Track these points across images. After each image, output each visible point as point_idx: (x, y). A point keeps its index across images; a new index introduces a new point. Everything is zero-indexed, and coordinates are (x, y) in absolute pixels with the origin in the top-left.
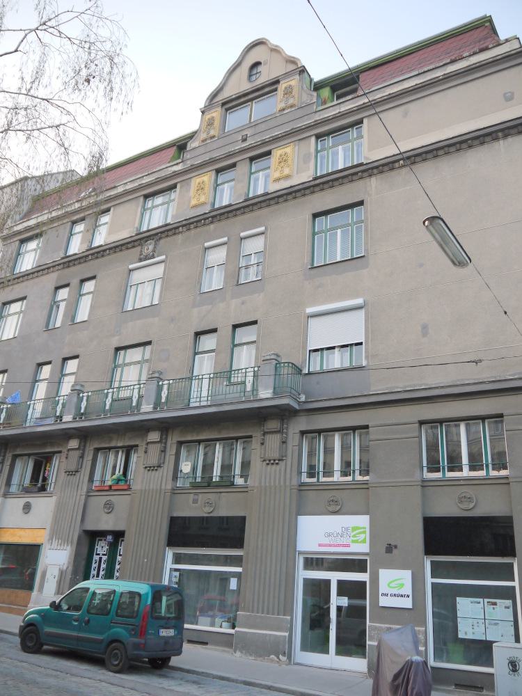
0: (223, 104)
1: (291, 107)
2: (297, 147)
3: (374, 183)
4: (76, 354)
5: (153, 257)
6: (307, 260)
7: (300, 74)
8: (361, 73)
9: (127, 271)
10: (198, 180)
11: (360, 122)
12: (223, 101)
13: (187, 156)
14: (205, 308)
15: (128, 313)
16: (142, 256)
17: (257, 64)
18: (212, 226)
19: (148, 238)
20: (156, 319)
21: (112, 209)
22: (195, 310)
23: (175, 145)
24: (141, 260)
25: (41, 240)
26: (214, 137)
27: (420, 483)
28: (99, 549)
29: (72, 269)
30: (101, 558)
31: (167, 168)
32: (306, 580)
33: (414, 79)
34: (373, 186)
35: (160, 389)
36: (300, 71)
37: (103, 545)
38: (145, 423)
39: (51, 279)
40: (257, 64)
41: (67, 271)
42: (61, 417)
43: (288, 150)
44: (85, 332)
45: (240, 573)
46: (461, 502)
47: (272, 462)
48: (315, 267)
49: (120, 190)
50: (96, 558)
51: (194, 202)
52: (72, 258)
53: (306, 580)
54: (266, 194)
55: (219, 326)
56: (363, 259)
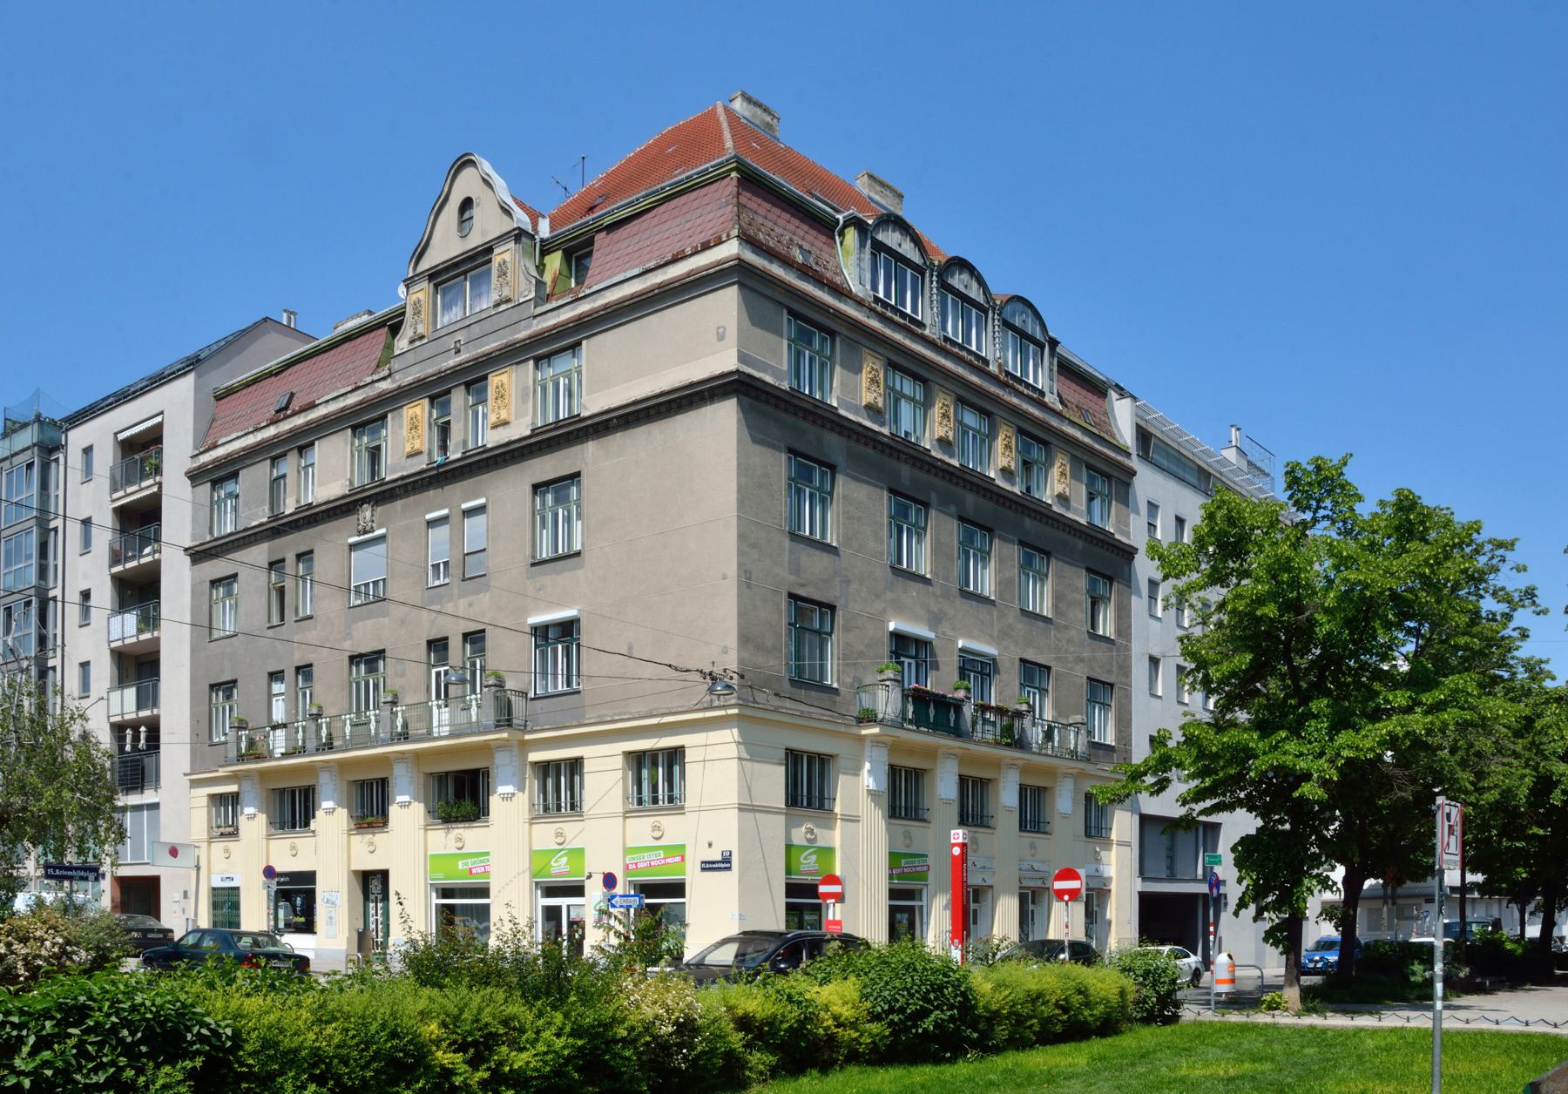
1: (508, 301)
2: (514, 375)
3: (591, 448)
4: (308, 663)
6: (528, 551)
8: (597, 232)
10: (411, 412)
11: (579, 344)
13: (396, 364)
16: (360, 527)
23: (384, 325)
26: (422, 337)
28: (374, 888)
32: (436, 905)
34: (590, 451)
35: (319, 727)
36: (515, 235)
43: (504, 378)
44: (314, 632)
46: (653, 831)
53: (436, 905)
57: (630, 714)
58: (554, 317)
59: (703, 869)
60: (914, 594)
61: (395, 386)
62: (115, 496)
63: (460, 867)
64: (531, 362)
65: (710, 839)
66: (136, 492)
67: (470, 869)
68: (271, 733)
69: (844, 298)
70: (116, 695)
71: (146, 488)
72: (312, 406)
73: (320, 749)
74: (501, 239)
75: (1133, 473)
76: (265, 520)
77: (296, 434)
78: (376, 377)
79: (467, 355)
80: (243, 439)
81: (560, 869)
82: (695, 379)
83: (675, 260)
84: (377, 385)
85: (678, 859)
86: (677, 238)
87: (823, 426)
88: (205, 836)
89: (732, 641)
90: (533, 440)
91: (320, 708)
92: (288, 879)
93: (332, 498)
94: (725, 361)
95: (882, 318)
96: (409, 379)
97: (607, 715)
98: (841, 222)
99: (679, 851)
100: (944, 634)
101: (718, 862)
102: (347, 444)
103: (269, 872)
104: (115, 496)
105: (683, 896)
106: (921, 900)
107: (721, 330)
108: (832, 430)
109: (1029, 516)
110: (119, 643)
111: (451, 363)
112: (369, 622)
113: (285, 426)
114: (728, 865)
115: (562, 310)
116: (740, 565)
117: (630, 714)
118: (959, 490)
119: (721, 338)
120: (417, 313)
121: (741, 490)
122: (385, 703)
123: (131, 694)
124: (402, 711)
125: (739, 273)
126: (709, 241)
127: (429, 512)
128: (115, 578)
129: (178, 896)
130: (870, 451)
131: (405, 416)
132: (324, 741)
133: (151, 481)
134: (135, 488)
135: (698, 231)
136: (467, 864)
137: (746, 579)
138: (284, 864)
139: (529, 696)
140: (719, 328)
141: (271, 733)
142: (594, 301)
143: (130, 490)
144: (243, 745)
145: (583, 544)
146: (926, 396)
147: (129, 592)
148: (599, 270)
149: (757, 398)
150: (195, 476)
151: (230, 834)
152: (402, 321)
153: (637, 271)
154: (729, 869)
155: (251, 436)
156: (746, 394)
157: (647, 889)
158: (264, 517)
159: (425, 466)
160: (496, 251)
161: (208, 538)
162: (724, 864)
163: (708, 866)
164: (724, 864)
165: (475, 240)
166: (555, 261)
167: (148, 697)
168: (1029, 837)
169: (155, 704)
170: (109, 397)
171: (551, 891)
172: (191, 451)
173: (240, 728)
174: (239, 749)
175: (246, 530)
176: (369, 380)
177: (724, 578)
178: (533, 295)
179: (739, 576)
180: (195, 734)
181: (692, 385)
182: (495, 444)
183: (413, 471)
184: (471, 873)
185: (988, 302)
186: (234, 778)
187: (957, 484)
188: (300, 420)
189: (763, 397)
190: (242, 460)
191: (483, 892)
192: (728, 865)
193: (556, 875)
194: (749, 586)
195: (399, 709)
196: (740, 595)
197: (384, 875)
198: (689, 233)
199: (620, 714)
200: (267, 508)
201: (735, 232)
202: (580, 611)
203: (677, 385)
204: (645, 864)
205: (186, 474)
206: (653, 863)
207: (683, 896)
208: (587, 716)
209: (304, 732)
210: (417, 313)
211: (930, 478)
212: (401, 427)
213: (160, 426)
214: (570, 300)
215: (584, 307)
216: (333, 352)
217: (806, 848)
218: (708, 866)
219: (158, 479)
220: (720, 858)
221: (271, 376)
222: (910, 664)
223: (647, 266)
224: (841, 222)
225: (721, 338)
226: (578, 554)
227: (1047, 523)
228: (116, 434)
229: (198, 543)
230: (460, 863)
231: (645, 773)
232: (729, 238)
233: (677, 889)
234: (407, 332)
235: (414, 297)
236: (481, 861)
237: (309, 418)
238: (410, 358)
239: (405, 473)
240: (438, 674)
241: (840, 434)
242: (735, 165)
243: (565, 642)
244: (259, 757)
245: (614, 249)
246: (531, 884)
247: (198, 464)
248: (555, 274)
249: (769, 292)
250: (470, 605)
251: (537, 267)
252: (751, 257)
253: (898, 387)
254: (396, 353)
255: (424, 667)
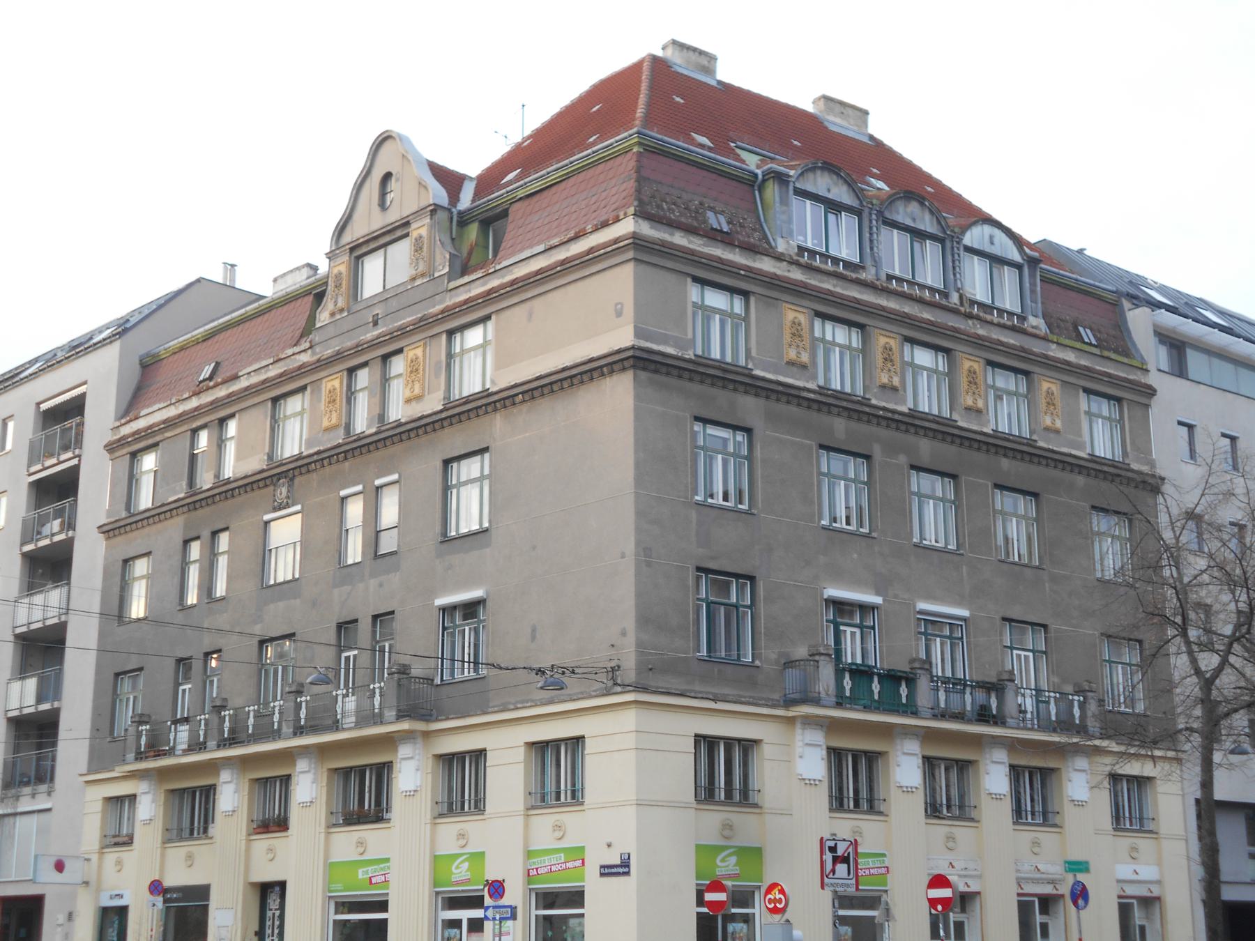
0: (352, 250)
5: (287, 506)
6: (438, 529)
7: (431, 215)
9: (262, 524)
10: (329, 385)
12: (351, 245)
13: (316, 337)
14: (347, 588)
15: (349, 569)
17: (388, 176)
18: (347, 464)
19: (279, 476)
20: (298, 601)
21: (493, 317)
22: (336, 591)
24: (275, 510)
25: (159, 452)
27: (635, 802)
29: (200, 512)
30: (274, 914)
31: (293, 354)
33: (540, 257)
34: (498, 426)
35: (222, 720)
36: (431, 211)
37: (274, 898)
38: (217, 761)
39: (174, 528)
40: (388, 176)
41: (194, 514)
42: (205, 743)
44: (225, 615)
45: (733, 907)
47: (408, 794)
48: (350, 565)
49: (243, 383)
50: (269, 914)
51: (326, 423)
52: (496, 398)
54: (485, 393)
55: (359, 616)
56: (224, 602)
57: (532, 701)
58: (466, 292)
59: (602, 875)
60: (855, 556)
61: (315, 358)
62: (33, 469)
63: (360, 876)
64: (444, 337)
65: (609, 840)
66: (53, 466)
67: (370, 878)
68: (173, 726)
69: (759, 256)
70: (16, 686)
71: (66, 460)
72: (236, 377)
73: (222, 744)
74: (418, 213)
75: (1150, 392)
76: (182, 495)
77: (215, 405)
78: (297, 349)
79: (384, 329)
80: (164, 410)
81: (461, 876)
82: (595, 354)
83: (576, 237)
84: (297, 357)
85: (579, 863)
86: (583, 212)
87: (735, 390)
88: (96, 846)
89: (630, 623)
90: (444, 415)
91: (225, 700)
92: (180, 895)
93: (250, 474)
94: (622, 337)
95: (809, 268)
96: (329, 352)
97: (510, 703)
98: (760, 177)
99: (578, 854)
100: (896, 596)
101: (616, 866)
102: (266, 419)
103: (156, 887)
104: (33, 469)
105: (582, 905)
106: (754, 908)
107: (619, 306)
108: (746, 392)
109: (1005, 456)
110: (24, 629)
111: (369, 336)
112: (281, 604)
113: (207, 398)
114: (626, 870)
115: (473, 285)
116: (638, 543)
117: (532, 701)
118: (911, 438)
119: (619, 314)
120: (338, 286)
121: (638, 465)
122: (289, 693)
123: (31, 684)
124: (306, 701)
125: (638, 243)
126: (608, 220)
127: (344, 488)
128: (25, 556)
129: (61, 918)
130: (794, 409)
131: (324, 389)
132: (226, 736)
133: (69, 455)
134: (54, 461)
135: (602, 206)
136: (367, 872)
137: (645, 555)
138: (177, 877)
139: (435, 682)
140: (616, 305)
141: (173, 726)
142: (503, 277)
143: (49, 462)
144: (143, 741)
145: (490, 522)
146: (864, 342)
147: (40, 571)
148: (511, 243)
149: (656, 371)
150: (111, 448)
151: (124, 844)
152: (325, 291)
153: (541, 248)
154: (627, 874)
155: (172, 407)
156: (644, 369)
157: (548, 899)
158: (181, 493)
159: (341, 441)
160: (414, 226)
161: (124, 514)
162: (621, 869)
163: (607, 871)
164: (621, 869)
165: (393, 216)
166: (473, 231)
167: (50, 688)
168: (940, 830)
169: (57, 696)
170: (36, 360)
171: (455, 902)
172: (112, 423)
173: (141, 723)
174: (139, 746)
175: (163, 505)
176: (290, 352)
177: (623, 556)
178: (447, 270)
179: (637, 554)
180: (96, 729)
181: (592, 360)
182: (408, 419)
183: (329, 446)
184: (371, 883)
185: (945, 232)
186: (133, 775)
187: (907, 431)
188: (221, 392)
189: (664, 369)
190: (163, 433)
191: (383, 906)
192: (626, 870)
193: (457, 883)
194: (649, 564)
195: (303, 699)
196: (638, 574)
197: (282, 885)
198: (594, 207)
199: (522, 702)
200: (184, 483)
201: (631, 210)
202: (487, 593)
203: (579, 360)
204: (546, 870)
205: (105, 447)
206: (554, 868)
207: (582, 906)
208: (491, 705)
209: (206, 725)
210: (338, 286)
211: (872, 429)
212: (320, 401)
213: (82, 397)
214: (481, 275)
215: (494, 283)
216: (260, 319)
217: (723, 848)
218: (607, 871)
219: (77, 452)
220: (618, 862)
221: (198, 343)
222: (853, 634)
223: (552, 243)
224: (760, 177)
225: (619, 314)
226: (487, 530)
227: (1031, 461)
228: (38, 404)
229: (113, 520)
230: (360, 871)
231: (282, 814)
232: (626, 216)
233: (576, 898)
234: (328, 305)
235: (335, 271)
236: (382, 869)
237: (231, 390)
238: (331, 331)
239: (322, 448)
240: (347, 658)
241: (756, 395)
242: (636, 140)
243: (472, 623)
244: (160, 754)
245: (527, 222)
246: (524, 891)
247: (118, 437)
248: (471, 245)
249: (669, 264)
250: (381, 585)
251: (453, 239)
252: (646, 229)
253: (829, 337)
254: (318, 325)
255: (333, 650)
